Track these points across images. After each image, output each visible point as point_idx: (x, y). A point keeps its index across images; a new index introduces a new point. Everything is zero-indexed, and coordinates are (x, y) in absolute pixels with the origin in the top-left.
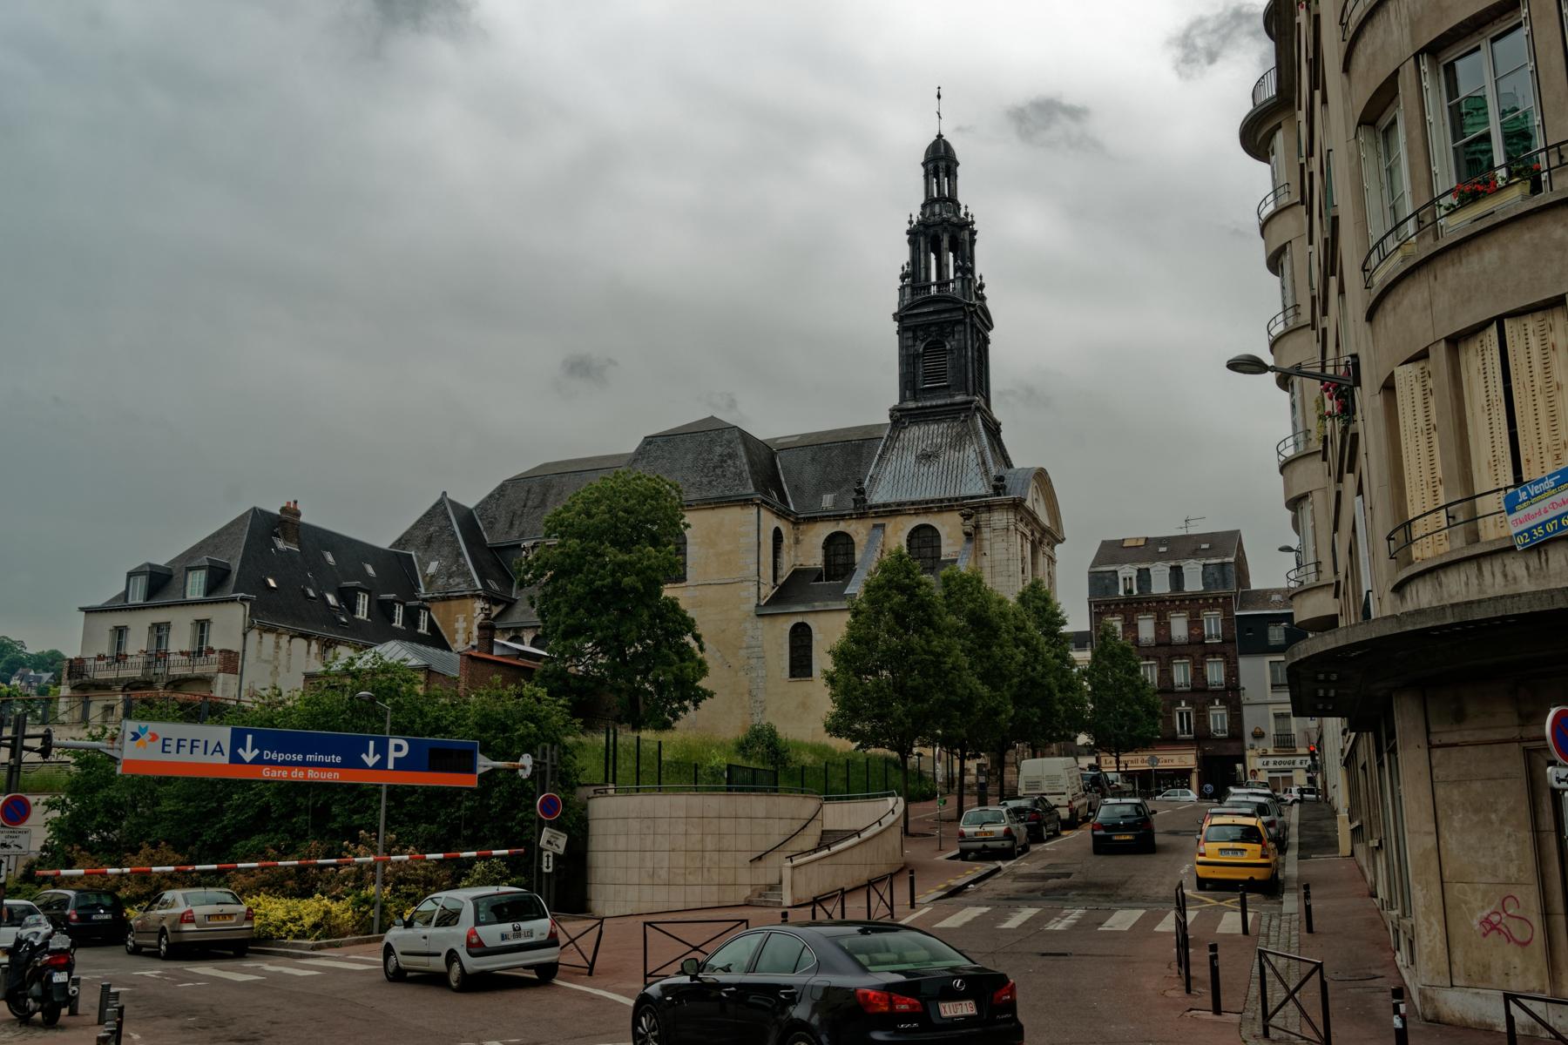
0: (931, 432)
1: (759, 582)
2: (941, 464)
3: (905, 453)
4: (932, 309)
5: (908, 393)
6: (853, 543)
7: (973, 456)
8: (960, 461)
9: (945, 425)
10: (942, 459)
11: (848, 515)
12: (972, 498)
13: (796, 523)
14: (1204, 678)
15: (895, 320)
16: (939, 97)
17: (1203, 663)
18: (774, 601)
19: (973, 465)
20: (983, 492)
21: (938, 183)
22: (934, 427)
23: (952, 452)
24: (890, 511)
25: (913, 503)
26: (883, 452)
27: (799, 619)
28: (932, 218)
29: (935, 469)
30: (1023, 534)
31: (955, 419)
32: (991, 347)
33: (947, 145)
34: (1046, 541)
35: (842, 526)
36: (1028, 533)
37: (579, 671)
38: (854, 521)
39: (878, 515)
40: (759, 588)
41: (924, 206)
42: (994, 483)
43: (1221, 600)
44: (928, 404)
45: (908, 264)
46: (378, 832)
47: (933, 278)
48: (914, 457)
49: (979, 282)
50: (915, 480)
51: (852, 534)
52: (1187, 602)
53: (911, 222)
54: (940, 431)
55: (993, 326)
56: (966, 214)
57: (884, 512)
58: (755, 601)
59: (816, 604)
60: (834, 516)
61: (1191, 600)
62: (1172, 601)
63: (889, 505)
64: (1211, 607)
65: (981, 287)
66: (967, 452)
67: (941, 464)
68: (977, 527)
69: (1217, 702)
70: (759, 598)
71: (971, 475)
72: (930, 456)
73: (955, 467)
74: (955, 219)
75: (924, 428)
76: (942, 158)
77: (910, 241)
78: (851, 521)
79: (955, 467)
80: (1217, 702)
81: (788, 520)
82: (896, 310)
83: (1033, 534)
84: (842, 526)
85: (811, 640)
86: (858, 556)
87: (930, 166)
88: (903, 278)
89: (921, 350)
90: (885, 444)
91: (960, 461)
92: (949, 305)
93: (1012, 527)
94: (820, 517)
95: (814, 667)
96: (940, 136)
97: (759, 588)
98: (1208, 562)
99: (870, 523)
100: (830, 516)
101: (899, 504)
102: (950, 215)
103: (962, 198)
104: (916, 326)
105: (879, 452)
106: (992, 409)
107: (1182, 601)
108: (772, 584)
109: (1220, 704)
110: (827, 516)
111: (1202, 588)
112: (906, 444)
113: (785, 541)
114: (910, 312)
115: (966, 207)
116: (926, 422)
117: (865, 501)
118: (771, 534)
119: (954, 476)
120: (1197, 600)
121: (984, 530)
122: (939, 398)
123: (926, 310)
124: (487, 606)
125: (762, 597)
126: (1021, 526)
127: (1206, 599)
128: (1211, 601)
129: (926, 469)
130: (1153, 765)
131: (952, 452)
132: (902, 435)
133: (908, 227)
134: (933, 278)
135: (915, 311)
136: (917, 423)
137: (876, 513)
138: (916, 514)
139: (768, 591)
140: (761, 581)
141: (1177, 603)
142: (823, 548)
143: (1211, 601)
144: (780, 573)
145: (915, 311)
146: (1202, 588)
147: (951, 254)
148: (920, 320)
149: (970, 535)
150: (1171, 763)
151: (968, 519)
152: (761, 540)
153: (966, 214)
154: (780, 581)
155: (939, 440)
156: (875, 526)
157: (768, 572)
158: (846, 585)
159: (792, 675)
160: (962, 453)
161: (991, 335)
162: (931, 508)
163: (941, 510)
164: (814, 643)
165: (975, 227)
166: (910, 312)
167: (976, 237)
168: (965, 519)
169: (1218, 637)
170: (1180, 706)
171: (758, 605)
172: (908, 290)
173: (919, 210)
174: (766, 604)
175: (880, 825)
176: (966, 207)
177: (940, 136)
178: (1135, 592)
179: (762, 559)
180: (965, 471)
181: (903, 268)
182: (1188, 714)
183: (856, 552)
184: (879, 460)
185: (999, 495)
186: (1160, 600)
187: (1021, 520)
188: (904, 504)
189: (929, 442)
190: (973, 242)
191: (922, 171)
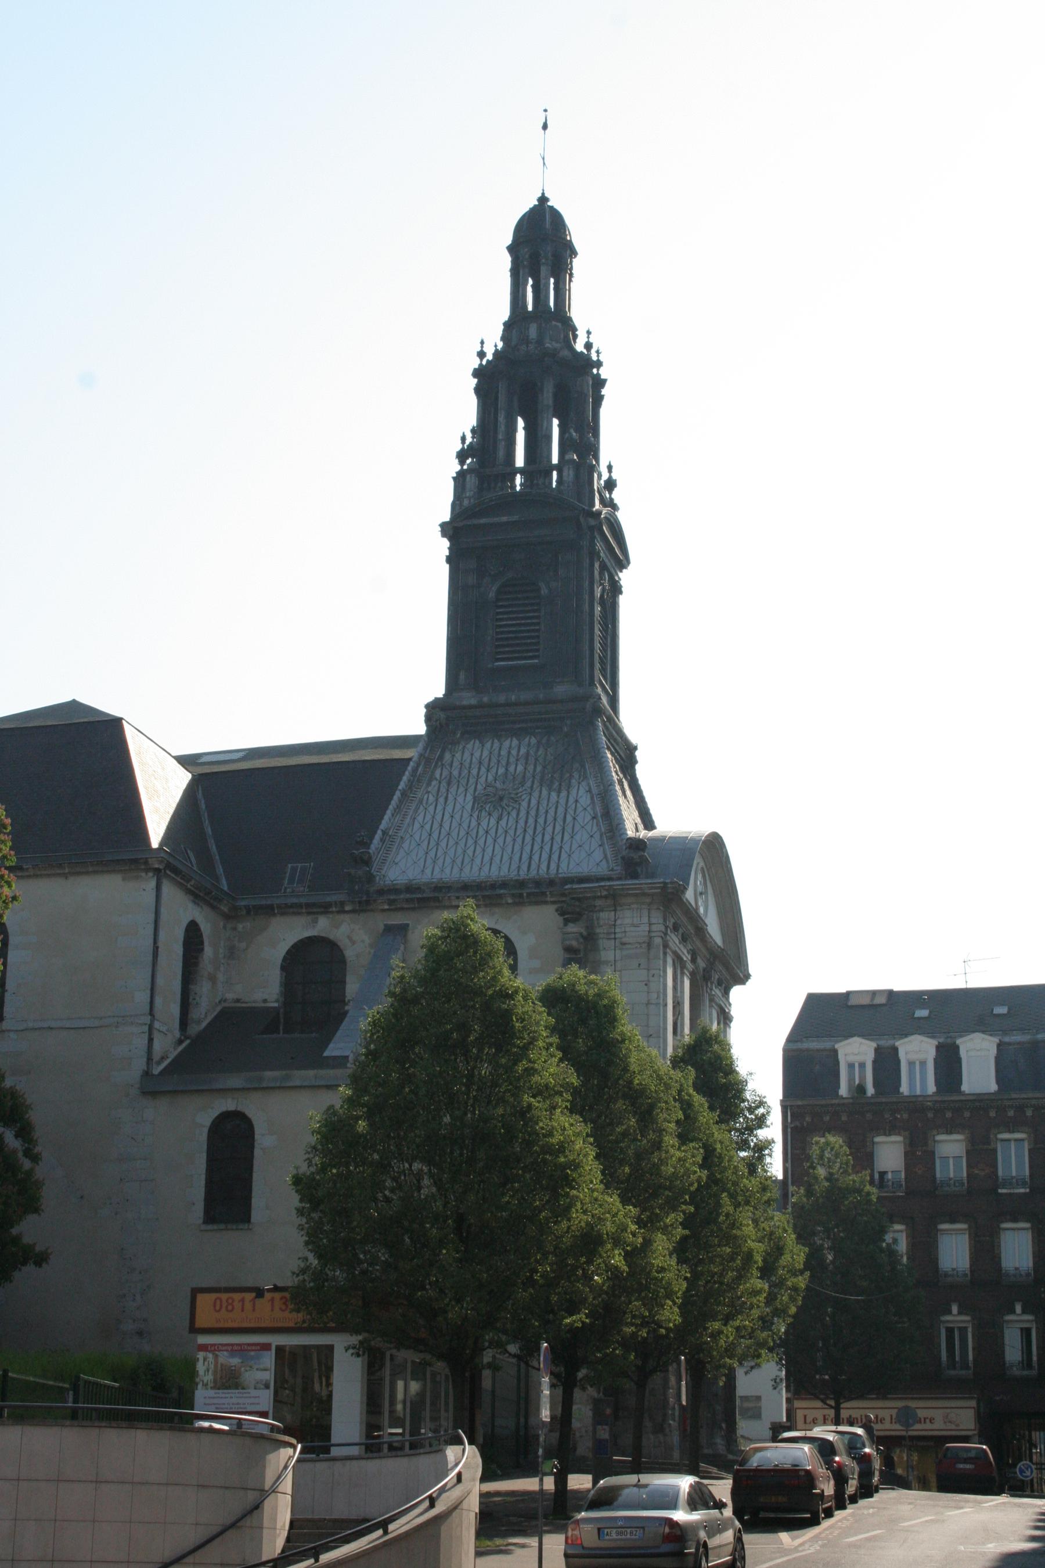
0: (504, 753)
1: (151, 1028)
2: (523, 813)
3: (453, 790)
4: (515, 518)
5: (462, 676)
6: (343, 961)
7: (585, 800)
8: (561, 810)
9: (534, 740)
10: (524, 804)
12: (582, 880)
13: (231, 916)
14: (934, 1261)
15: (444, 534)
16: (545, 127)
17: (994, 1233)
18: (177, 1066)
19: (584, 818)
20: (603, 870)
21: (536, 289)
22: (510, 744)
23: (545, 792)
24: (420, 900)
26: (410, 785)
27: (228, 1104)
28: (524, 347)
29: (512, 821)
30: (678, 960)
32: (623, 601)
33: (557, 219)
34: (715, 977)
35: (321, 926)
36: (686, 957)
37: (500, 1130)
38: (347, 917)
39: (395, 907)
40: (151, 1040)
41: (508, 326)
42: (624, 853)
43: (1029, 1113)
44: (502, 699)
45: (473, 431)
47: (520, 461)
48: (469, 797)
49: (605, 476)
53: (481, 354)
54: (523, 751)
55: (629, 562)
56: (588, 346)
57: (407, 901)
58: (139, 1065)
59: (268, 1074)
60: (308, 905)
64: (1011, 1126)
65: (611, 485)
66: (574, 792)
67: (523, 813)
68: (590, 938)
69: (1018, 1308)
70: (149, 1059)
72: (501, 799)
73: (550, 818)
74: (565, 353)
75: (491, 745)
77: (478, 390)
78: (342, 916)
79: (550, 818)
80: (1018, 1308)
81: (213, 907)
82: (446, 517)
83: (694, 960)
84: (321, 926)
85: (252, 1147)
86: (352, 987)
87: (525, 252)
88: (462, 456)
89: (492, 595)
90: (415, 770)
91: (561, 810)
93: (658, 941)
94: (279, 907)
95: (255, 1201)
97: (151, 1040)
98: (1007, 1039)
99: (380, 921)
100: (300, 906)
102: (557, 345)
103: (580, 312)
105: (402, 785)
106: (621, 718)
108: (177, 1034)
109: (1024, 1312)
110: (293, 906)
112: (455, 773)
113: (208, 951)
114: (476, 521)
115: (589, 333)
117: (370, 878)
118: (180, 933)
119: (547, 838)
121: (602, 943)
123: (504, 519)
124: (558, 1419)
125: (156, 1057)
126: (674, 940)
128: (949, 1115)
129: (493, 821)
130: (907, 1431)
131: (545, 792)
132: (447, 756)
133: (476, 363)
134: (520, 461)
135: (483, 521)
139: (167, 1046)
140: (157, 1025)
141: (949, 1115)
142: (283, 968)
143: (1011, 1113)
144: (195, 1014)
145: (483, 521)
147: (555, 422)
149: (576, 951)
150: (928, 1426)
151: (574, 921)
152: (160, 944)
153: (588, 346)
154: (194, 1029)
155: (520, 768)
156: (389, 929)
157: (170, 1008)
158: (325, 1044)
159: (210, 1217)
160: (564, 794)
161: (625, 577)
162: (500, 896)
163: (520, 901)
164: (257, 1152)
165: (604, 373)
166: (476, 521)
167: (604, 392)
168: (566, 922)
169: (1024, 1184)
170: (950, 1312)
171: (147, 1074)
172: (471, 481)
173: (499, 330)
174: (162, 1073)
175: (386, 1532)
176: (589, 333)
177: (543, 200)
178: (870, 1090)
179: (160, 981)
180: (569, 829)
181: (463, 439)
182: (963, 1331)
183: (349, 978)
184: (400, 801)
185: (635, 876)
186: (916, 1106)
187: (675, 928)
189: (501, 771)
190: (598, 400)
191: (507, 260)
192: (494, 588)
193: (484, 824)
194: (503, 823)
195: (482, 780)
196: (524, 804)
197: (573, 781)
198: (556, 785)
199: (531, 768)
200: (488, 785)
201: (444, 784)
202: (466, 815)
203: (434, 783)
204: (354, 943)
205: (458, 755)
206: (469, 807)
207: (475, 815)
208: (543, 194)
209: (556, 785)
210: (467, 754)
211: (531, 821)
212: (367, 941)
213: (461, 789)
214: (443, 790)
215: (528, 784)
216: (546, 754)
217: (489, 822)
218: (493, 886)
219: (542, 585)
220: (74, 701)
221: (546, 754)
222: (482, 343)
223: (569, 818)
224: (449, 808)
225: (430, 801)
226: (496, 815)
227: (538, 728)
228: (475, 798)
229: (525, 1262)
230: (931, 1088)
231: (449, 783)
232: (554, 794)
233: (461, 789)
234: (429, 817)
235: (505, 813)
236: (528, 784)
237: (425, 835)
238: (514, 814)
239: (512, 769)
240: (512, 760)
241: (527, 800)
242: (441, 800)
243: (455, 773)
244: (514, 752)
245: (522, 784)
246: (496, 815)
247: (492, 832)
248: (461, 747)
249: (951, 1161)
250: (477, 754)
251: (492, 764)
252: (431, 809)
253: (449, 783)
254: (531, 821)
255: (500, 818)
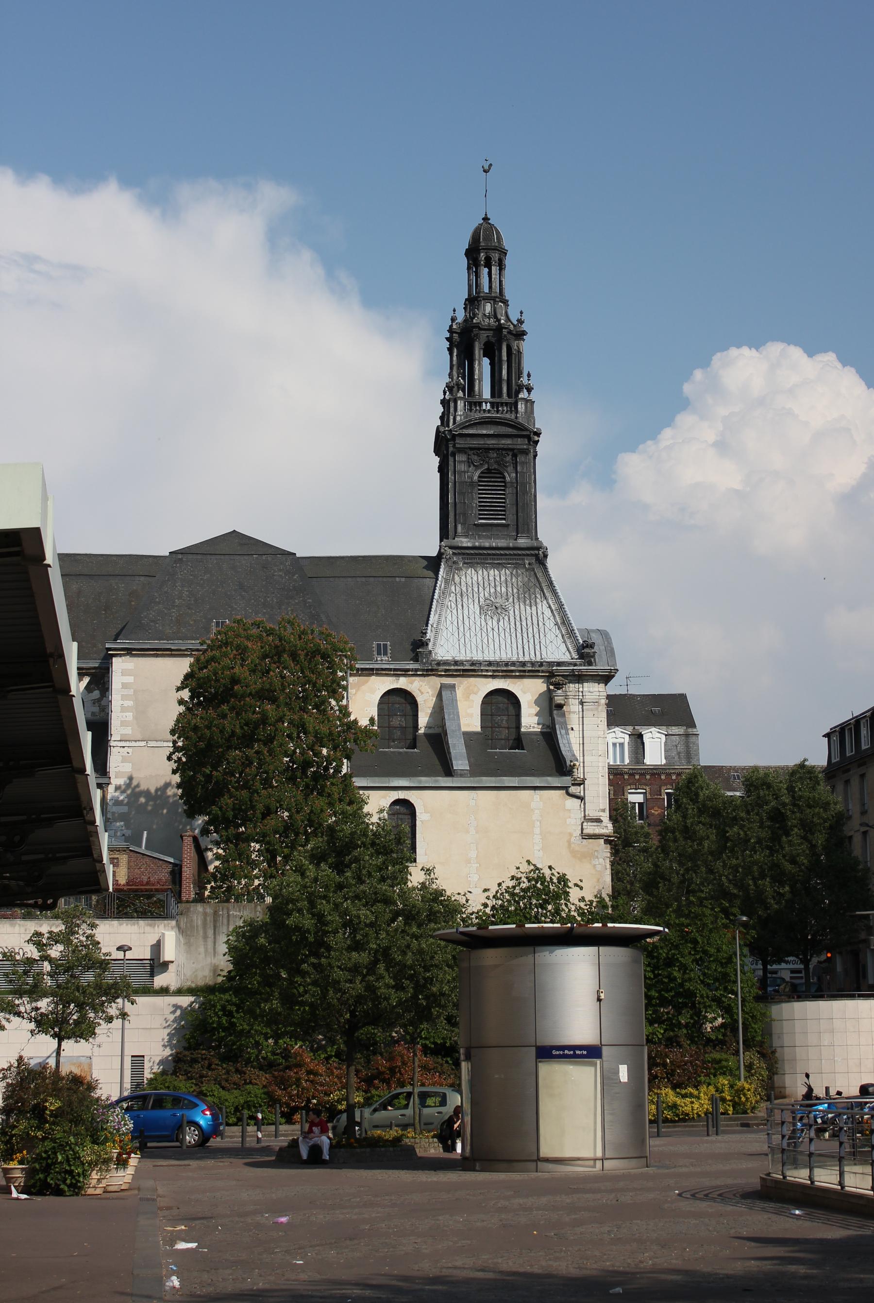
0: (491, 578)
2: (512, 619)
3: (465, 599)
4: (491, 432)
7: (548, 613)
8: (535, 618)
10: (511, 612)
11: (412, 670)
19: (550, 624)
24: (464, 670)
25: (490, 663)
31: (517, 566)
35: (402, 683)
39: (449, 674)
46: (744, 1065)
48: (477, 606)
50: (484, 635)
51: (416, 694)
52: (648, 777)
57: (457, 670)
61: (653, 775)
62: (632, 775)
63: (461, 663)
66: (539, 606)
67: (512, 619)
71: (550, 636)
76: (495, 249)
77: (490, 364)
84: (402, 683)
89: (476, 478)
92: (514, 432)
94: (377, 669)
96: (486, 219)
101: (473, 663)
104: (471, 449)
107: (642, 775)
111: (664, 762)
112: (464, 589)
116: (484, 565)
120: (659, 775)
122: (497, 537)
123: (484, 432)
127: (669, 775)
128: (637, 777)
129: (495, 623)
131: (522, 606)
132: (457, 578)
135: (471, 431)
136: (471, 565)
137: (446, 671)
138: (493, 677)
141: (637, 777)
143: (674, 777)
146: (664, 762)
148: (475, 442)
155: (504, 589)
160: (534, 608)
177: (486, 219)
180: (542, 630)
188: (480, 663)
192: (477, 474)
193: (490, 623)
194: (501, 623)
195: (482, 595)
196: (511, 612)
197: (538, 600)
198: (528, 602)
199: (510, 590)
200: (486, 599)
201: (459, 596)
202: (477, 617)
203: (452, 595)
204: (422, 693)
205: (463, 577)
206: (478, 612)
207: (483, 617)
208: (486, 215)
209: (528, 602)
210: (468, 578)
211: (518, 624)
212: (431, 693)
213: (470, 600)
214: (459, 600)
215: (511, 600)
216: (517, 582)
217: (492, 623)
218: (507, 664)
219: (506, 474)
220: (234, 534)
221: (517, 582)
222: (454, 310)
223: (541, 624)
224: (466, 612)
225: (453, 607)
226: (495, 618)
227: (509, 564)
228: (480, 606)
229: (397, 867)
230: (627, 761)
231: (462, 595)
232: (528, 608)
233: (470, 600)
234: (454, 617)
235: (501, 618)
236: (511, 600)
237: (455, 629)
238: (506, 618)
239: (498, 589)
240: (497, 583)
241: (512, 610)
242: (460, 606)
243: (464, 589)
244: (498, 578)
245: (507, 599)
246: (495, 618)
247: (496, 629)
248: (464, 573)
249: (637, 805)
250: (475, 578)
251: (485, 586)
252: (455, 611)
253: (462, 595)
254: (518, 624)
255: (499, 621)
